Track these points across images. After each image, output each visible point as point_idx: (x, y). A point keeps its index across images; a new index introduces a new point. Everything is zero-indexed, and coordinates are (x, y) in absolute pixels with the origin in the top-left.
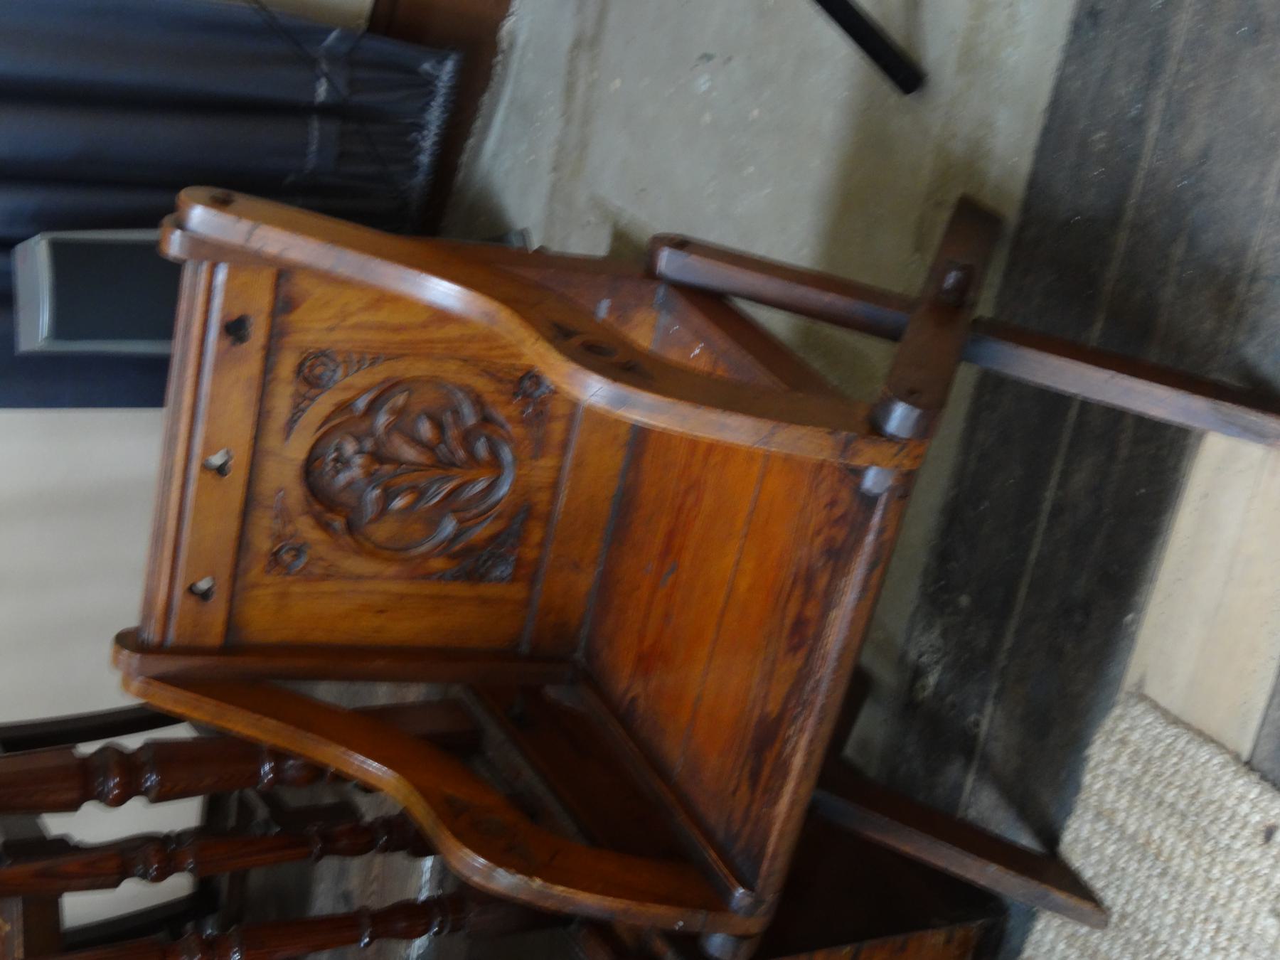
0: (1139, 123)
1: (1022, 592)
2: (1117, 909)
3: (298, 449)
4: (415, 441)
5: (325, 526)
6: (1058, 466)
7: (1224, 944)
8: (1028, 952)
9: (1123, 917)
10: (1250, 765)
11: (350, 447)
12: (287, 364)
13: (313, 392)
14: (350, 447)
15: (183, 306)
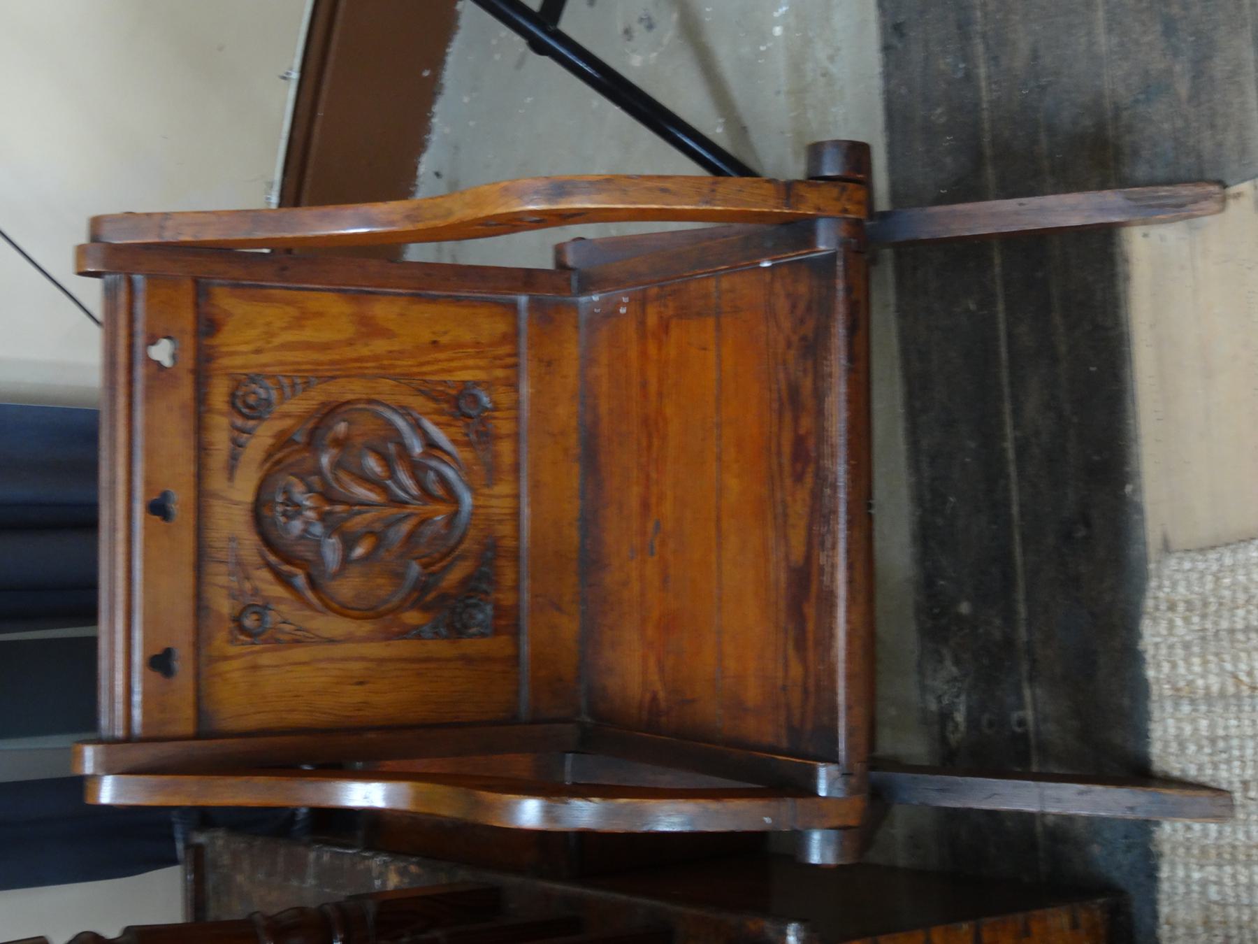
1: (1018, 550)
2: (1237, 786)
3: (244, 489)
5: (284, 580)
6: (1007, 407)
8: (1164, 931)
9: (1245, 784)
11: (299, 493)
12: (219, 394)
13: (251, 423)
14: (299, 493)
15: (103, 665)
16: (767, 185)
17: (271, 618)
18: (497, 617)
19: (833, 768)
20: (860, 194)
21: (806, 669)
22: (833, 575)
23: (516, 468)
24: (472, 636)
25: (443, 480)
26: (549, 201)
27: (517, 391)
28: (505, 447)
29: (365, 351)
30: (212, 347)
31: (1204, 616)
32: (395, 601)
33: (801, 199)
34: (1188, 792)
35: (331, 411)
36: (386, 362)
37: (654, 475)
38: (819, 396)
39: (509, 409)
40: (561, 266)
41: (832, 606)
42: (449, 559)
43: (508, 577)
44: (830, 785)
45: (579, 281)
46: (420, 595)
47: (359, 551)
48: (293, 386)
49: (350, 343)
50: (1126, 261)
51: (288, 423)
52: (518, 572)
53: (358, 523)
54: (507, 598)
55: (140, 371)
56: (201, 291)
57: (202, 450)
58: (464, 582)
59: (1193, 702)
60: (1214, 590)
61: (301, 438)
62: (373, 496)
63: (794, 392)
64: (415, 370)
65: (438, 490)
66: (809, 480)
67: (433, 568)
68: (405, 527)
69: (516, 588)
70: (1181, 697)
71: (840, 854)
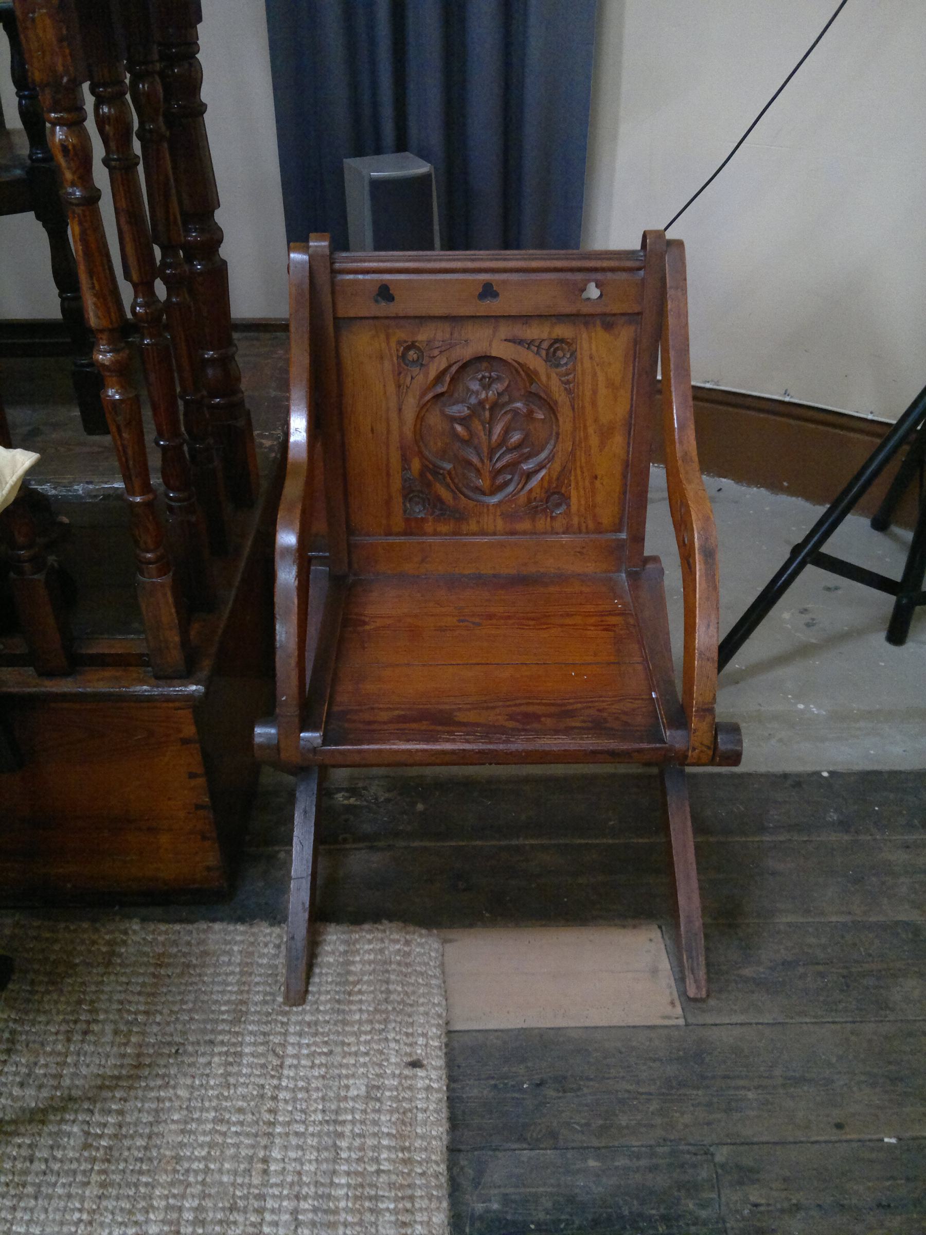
0: (762, 829)
3: (499, 350)
4: (507, 431)
7: (317, 1062)
10: (449, 1033)
11: (499, 387)
12: (563, 331)
13: (543, 353)
14: (499, 387)
16: (711, 695)
17: (415, 370)
18: (416, 519)
19: (320, 741)
20: (704, 758)
21: (385, 723)
22: (448, 741)
23: (513, 533)
24: (404, 503)
25: (506, 484)
26: (701, 547)
27: (564, 533)
28: (526, 525)
29: (591, 430)
30: (595, 326)
31: (399, 964)
32: (427, 453)
33: (703, 718)
34: (304, 976)
35: (551, 408)
36: (583, 445)
37: (510, 622)
38: (567, 731)
39: (552, 527)
40: (647, 560)
41: (427, 741)
42: (454, 488)
43: (444, 528)
44: (307, 740)
45: (636, 572)
46: (431, 471)
47: (459, 428)
48: (568, 382)
49: (596, 420)
50: (634, 927)
51: (544, 378)
52: (446, 535)
53: (477, 426)
54: (429, 527)
55: (579, 276)
56: (634, 317)
57: (525, 319)
58: (439, 499)
59: (346, 952)
60: (416, 971)
61: (533, 389)
62: (495, 437)
63: (570, 714)
64: (578, 464)
65: (500, 480)
66: (511, 724)
67: (448, 478)
68: (475, 460)
69: (435, 533)
70: (349, 945)
71: (261, 746)
